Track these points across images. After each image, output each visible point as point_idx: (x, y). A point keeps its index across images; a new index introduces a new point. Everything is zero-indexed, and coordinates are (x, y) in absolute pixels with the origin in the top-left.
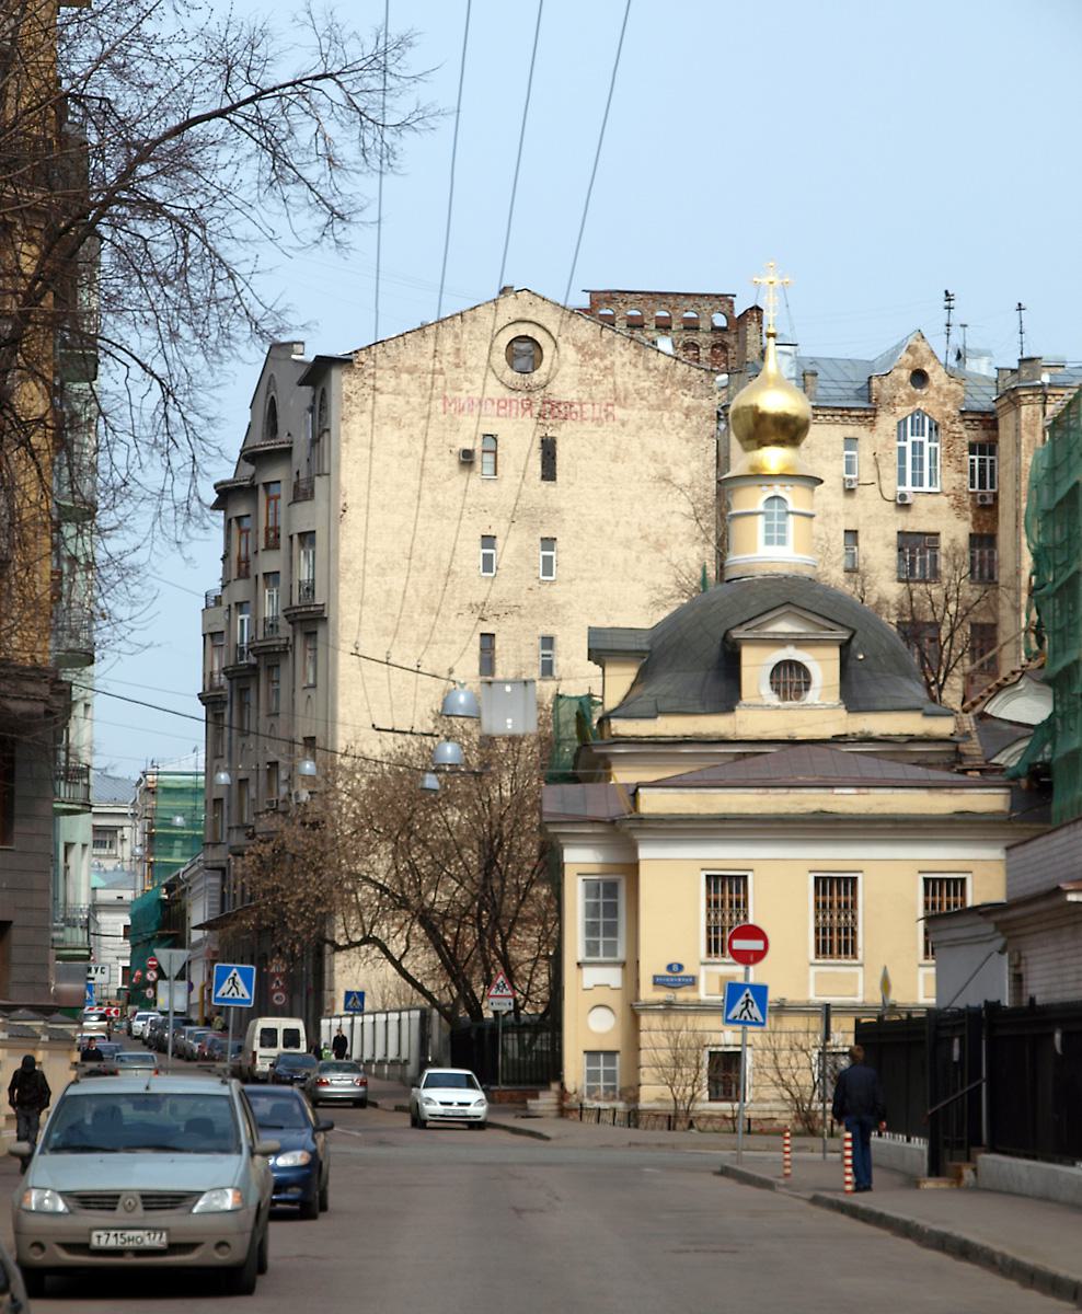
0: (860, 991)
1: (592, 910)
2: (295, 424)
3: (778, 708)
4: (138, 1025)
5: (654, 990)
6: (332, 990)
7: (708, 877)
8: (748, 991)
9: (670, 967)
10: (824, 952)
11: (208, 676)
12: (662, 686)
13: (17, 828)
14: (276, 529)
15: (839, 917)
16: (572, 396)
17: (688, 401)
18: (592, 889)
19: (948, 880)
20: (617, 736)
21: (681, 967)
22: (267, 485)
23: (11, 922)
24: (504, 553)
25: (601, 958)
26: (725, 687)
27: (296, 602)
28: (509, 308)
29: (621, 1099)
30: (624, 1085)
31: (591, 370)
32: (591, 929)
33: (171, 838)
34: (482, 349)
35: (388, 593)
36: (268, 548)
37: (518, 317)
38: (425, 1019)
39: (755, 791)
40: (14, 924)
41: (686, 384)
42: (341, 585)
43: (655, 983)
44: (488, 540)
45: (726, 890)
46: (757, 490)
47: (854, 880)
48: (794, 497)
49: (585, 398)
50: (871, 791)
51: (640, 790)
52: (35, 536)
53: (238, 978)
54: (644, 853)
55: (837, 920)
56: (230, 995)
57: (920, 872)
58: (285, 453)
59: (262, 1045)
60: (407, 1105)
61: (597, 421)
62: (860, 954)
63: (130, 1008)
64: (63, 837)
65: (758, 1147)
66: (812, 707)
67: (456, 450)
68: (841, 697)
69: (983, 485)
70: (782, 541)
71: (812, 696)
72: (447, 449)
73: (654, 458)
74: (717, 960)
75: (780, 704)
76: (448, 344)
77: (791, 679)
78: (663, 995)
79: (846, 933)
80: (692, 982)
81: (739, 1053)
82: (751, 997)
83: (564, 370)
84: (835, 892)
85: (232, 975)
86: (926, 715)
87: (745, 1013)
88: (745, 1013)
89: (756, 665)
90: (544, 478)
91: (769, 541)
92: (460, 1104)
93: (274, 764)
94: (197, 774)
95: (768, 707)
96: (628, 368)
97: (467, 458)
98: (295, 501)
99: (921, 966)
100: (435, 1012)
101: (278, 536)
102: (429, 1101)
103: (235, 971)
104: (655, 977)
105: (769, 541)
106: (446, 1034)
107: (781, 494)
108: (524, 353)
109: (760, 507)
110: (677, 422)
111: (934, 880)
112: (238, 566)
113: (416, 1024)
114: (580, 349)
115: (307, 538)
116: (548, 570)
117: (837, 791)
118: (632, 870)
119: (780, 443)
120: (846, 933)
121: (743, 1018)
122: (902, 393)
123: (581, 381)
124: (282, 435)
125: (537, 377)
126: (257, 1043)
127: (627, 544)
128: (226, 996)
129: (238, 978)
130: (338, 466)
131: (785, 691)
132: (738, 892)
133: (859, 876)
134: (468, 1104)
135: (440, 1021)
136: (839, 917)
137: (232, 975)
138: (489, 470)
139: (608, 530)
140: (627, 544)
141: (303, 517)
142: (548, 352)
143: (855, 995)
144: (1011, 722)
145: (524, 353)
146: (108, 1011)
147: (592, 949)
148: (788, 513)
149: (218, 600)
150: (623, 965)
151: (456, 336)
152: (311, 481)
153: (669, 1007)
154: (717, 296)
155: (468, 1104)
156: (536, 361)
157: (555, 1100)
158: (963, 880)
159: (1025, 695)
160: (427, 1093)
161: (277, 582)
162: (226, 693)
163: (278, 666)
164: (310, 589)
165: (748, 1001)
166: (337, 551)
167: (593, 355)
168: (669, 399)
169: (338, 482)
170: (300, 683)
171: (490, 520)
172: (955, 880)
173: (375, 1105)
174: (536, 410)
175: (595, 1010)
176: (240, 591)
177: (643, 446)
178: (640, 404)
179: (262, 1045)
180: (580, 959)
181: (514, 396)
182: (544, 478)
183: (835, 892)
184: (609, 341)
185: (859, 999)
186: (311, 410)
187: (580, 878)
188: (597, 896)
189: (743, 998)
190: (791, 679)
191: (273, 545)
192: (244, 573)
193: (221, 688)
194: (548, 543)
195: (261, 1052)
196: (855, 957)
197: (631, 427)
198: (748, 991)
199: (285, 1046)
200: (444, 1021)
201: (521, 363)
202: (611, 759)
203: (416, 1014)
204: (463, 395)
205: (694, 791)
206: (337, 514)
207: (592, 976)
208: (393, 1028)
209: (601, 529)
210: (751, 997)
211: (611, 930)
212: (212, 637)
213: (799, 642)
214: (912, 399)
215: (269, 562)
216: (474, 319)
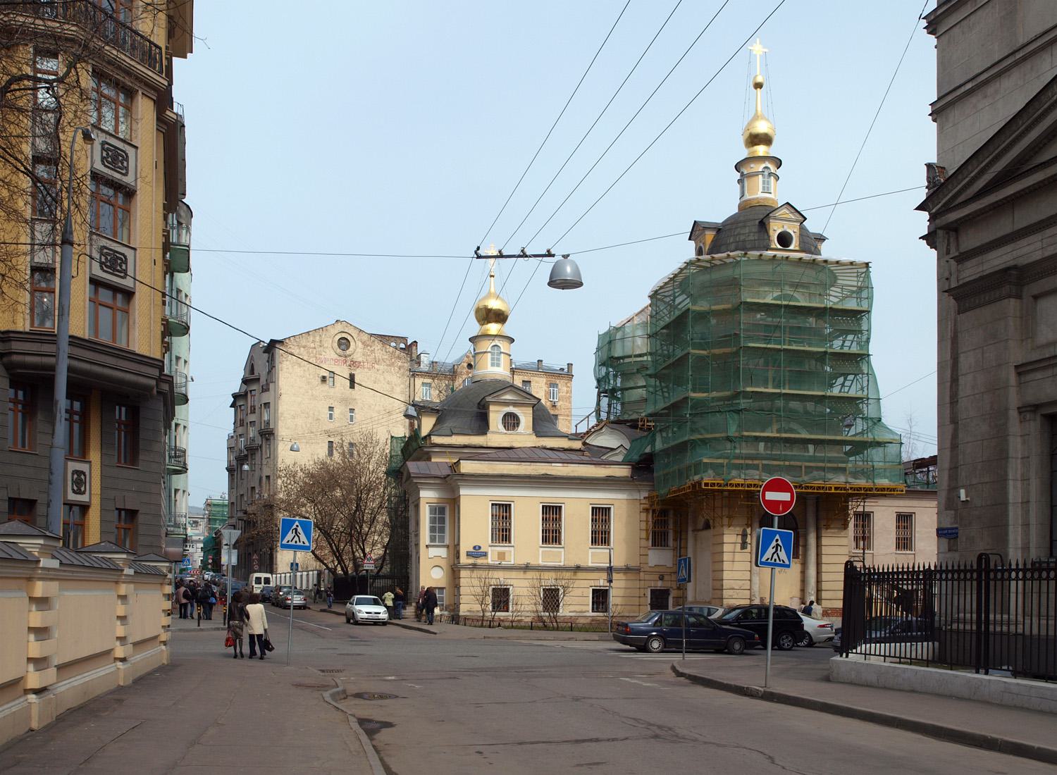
0: (563, 560)
1: (433, 521)
2: (261, 370)
3: (506, 434)
4: (206, 577)
5: (467, 558)
6: (276, 564)
7: (493, 504)
8: (777, 537)
9: (474, 548)
10: (546, 542)
11: (229, 462)
12: (449, 424)
13: (141, 457)
14: (254, 406)
15: (553, 525)
16: (360, 359)
18: (433, 510)
19: (603, 508)
20: (434, 444)
21: (480, 548)
22: (251, 391)
23: (138, 511)
24: (336, 413)
25: (437, 544)
26: (482, 425)
27: (263, 428)
28: (339, 327)
29: (446, 610)
30: (448, 603)
32: (432, 529)
33: (216, 520)
34: (330, 342)
35: (296, 425)
36: (251, 413)
37: (343, 330)
38: (320, 574)
39: (515, 463)
40: (140, 511)
41: (399, 358)
42: (280, 422)
43: (467, 555)
44: (331, 408)
45: (503, 511)
46: (489, 342)
47: (560, 507)
48: (503, 346)
49: (365, 360)
50: (569, 465)
51: (461, 461)
52: (92, 38)
53: (300, 529)
54: (463, 492)
55: (551, 526)
56: (293, 543)
57: (591, 504)
58: (258, 380)
59: (256, 583)
60: (344, 612)
61: (369, 369)
62: (563, 542)
63: (204, 571)
64: (174, 487)
65: (550, 638)
66: (521, 434)
67: (320, 376)
68: (533, 430)
69: (553, 398)
70: (498, 365)
71: (521, 429)
72: (316, 375)
74: (506, 545)
75: (506, 432)
76: (318, 338)
77: (511, 421)
78: (471, 561)
79: (556, 533)
80: (485, 554)
81: (607, 590)
82: (780, 542)
83: (357, 350)
84: (552, 513)
85: (294, 527)
86: (570, 439)
87: (775, 556)
88: (775, 556)
89: (496, 416)
90: (351, 388)
91: (493, 365)
92: (376, 613)
93: (253, 488)
94: (223, 506)
95: (501, 433)
97: (324, 379)
98: (262, 392)
99: (590, 548)
100: (327, 571)
101: (255, 409)
102: (360, 611)
103: (297, 523)
104: (467, 552)
105: (493, 365)
106: (331, 580)
107: (499, 344)
108: (344, 343)
109: (489, 350)
111: (596, 508)
112: (239, 423)
113: (315, 576)
114: (363, 343)
115: (267, 405)
116: (352, 420)
117: (553, 464)
118: (454, 502)
119: (497, 322)
120: (556, 533)
121: (773, 561)
122: (464, 371)
123: (363, 355)
124: (256, 374)
125: (348, 352)
126: (254, 582)
128: (290, 543)
129: (300, 529)
130: (278, 378)
131: (508, 427)
132: (506, 512)
133: (563, 505)
134: (379, 613)
135: (329, 574)
136: (553, 525)
137: (294, 527)
138: (331, 384)
139: (373, 407)
140: (379, 412)
141: (266, 398)
142: (352, 344)
143: (560, 562)
144: (598, 447)
145: (344, 343)
146: (80, 121)
147: (433, 539)
148: (501, 353)
149: (232, 437)
150: (448, 547)
151: (320, 336)
152: (268, 384)
153: (474, 567)
154: (402, 338)
155: (379, 613)
156: (348, 347)
157: (413, 611)
158: (609, 509)
159: (605, 435)
160: (358, 607)
161: (254, 425)
162: (235, 467)
163: (255, 454)
164: (268, 423)
165: (778, 545)
166: (278, 410)
167: (368, 346)
169: (278, 385)
170: (264, 457)
171: (332, 401)
172: (606, 508)
173: (309, 608)
174: (348, 364)
175: (437, 568)
176: (240, 430)
177: (385, 378)
178: (383, 363)
179: (256, 583)
180: (427, 544)
181: (340, 358)
182: (351, 388)
183: (552, 513)
184: (374, 341)
185: (562, 564)
186: (268, 361)
187: (427, 505)
188: (435, 514)
189: (774, 543)
190: (511, 421)
191: (253, 412)
192: (242, 425)
193: (233, 466)
194: (352, 410)
195: (256, 586)
196: (560, 544)
197: (380, 372)
198: (777, 537)
199: (265, 584)
200: (331, 574)
201: (343, 347)
202: (431, 454)
203: (315, 572)
204: (322, 357)
205: (487, 462)
206: (278, 397)
207: (433, 552)
208: (304, 578)
209: (370, 407)
210: (780, 542)
211: (442, 530)
212: (230, 449)
213: (515, 404)
214: (468, 373)
215: (252, 418)
216: (327, 330)
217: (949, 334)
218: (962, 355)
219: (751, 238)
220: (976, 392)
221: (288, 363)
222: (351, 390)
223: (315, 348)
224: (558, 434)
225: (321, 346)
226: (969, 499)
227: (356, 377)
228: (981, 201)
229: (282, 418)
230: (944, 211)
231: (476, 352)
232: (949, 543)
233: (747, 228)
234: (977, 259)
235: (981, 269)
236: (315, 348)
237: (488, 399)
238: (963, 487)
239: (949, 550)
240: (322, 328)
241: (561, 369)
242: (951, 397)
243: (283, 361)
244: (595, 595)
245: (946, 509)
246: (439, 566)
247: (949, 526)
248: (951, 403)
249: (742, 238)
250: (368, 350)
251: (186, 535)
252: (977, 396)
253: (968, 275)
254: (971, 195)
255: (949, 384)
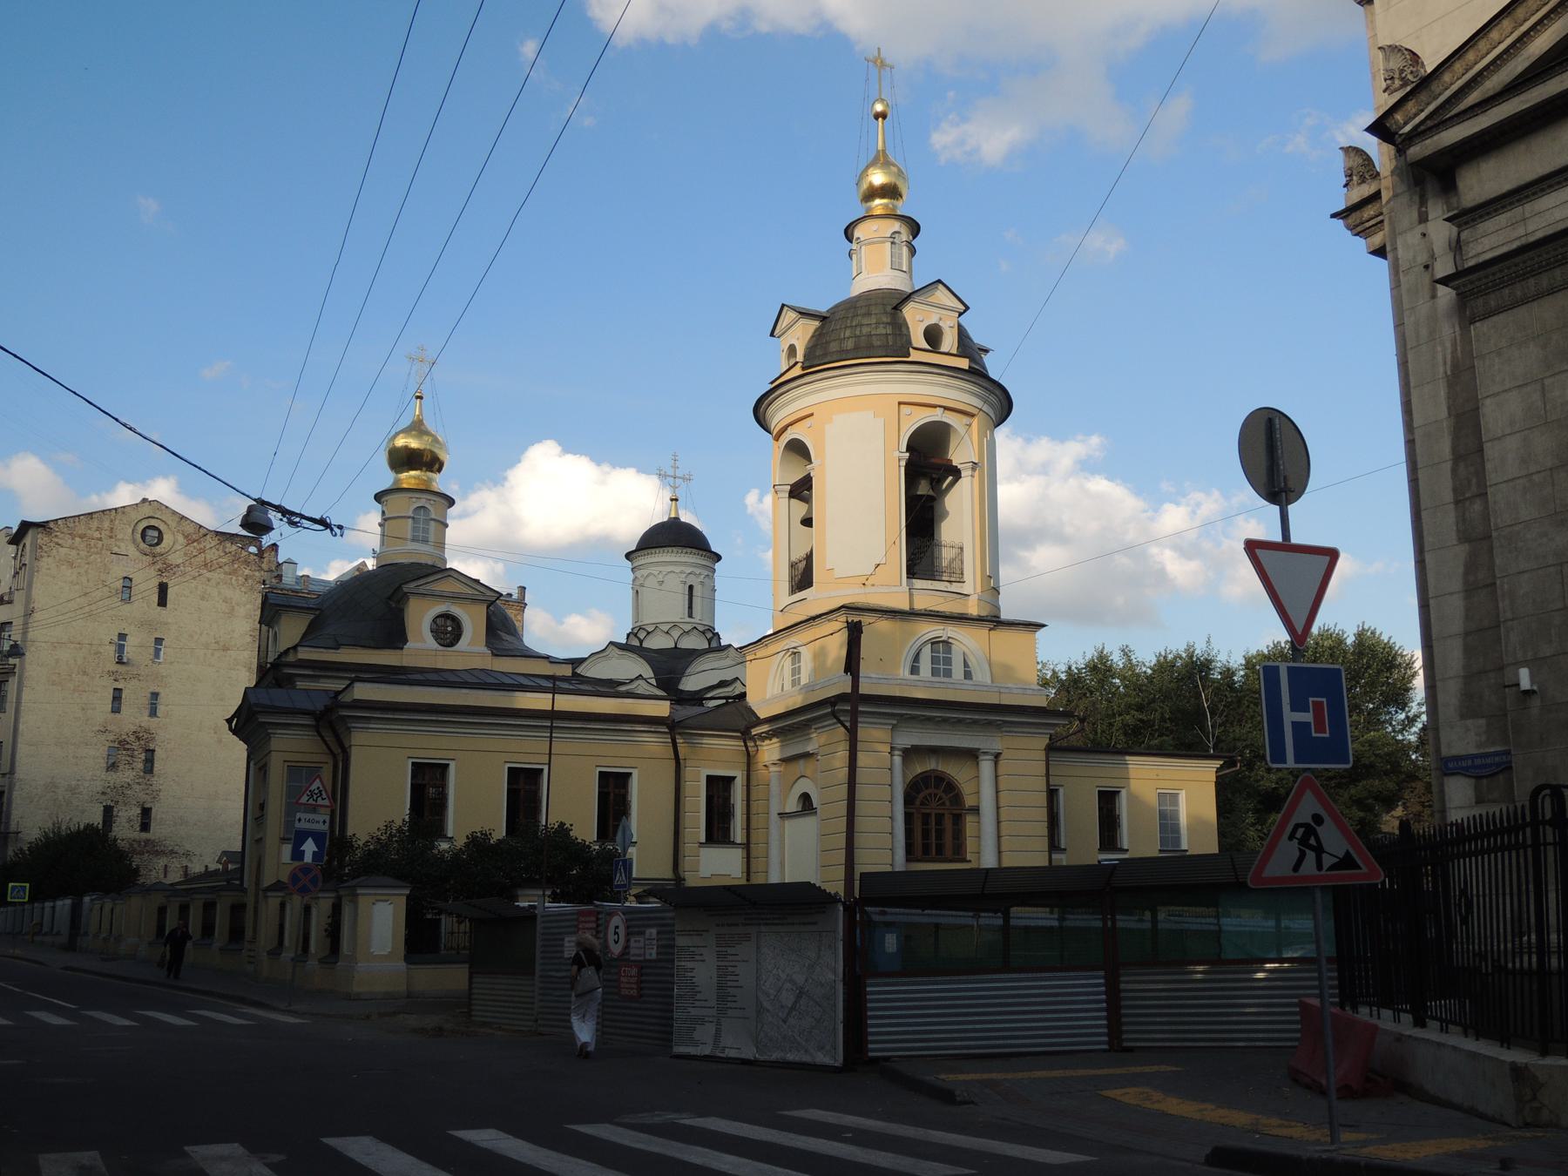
17: (247, 572)
26: (395, 636)
31: (192, 549)
35: (57, 661)
71: (463, 644)
73: (225, 601)
96: (214, 550)
109: (410, 514)
110: (240, 582)
114: (186, 537)
125: (158, 549)
127: (207, 646)
140: (207, 646)
151: (112, 521)
168: (236, 570)
177: (219, 593)
194: (159, 641)
209: (191, 636)
217: (1441, 369)
218: (1488, 402)
219: (881, 330)
220: (1533, 469)
221: (50, 560)
222: (159, 608)
223: (100, 539)
224: (528, 654)
225: (111, 537)
226: (1535, 688)
227: (169, 591)
228: (1523, 97)
229: (33, 649)
230: (1430, 129)
231: (387, 516)
232: (1477, 789)
233: (873, 316)
234: (1509, 214)
235: (1521, 231)
236: (100, 539)
237: (406, 588)
238: (1525, 664)
239: (1477, 803)
240: (116, 509)
241: (508, 594)
242: (1455, 490)
243: (42, 557)
244: (847, 970)
245: (1463, 717)
246: (799, 778)
247: (1474, 751)
248: (1457, 502)
249: (865, 330)
250: (195, 548)
251: (1219, 926)
252: (1536, 478)
253: (1487, 247)
254: (1498, 89)
255: (1448, 466)
